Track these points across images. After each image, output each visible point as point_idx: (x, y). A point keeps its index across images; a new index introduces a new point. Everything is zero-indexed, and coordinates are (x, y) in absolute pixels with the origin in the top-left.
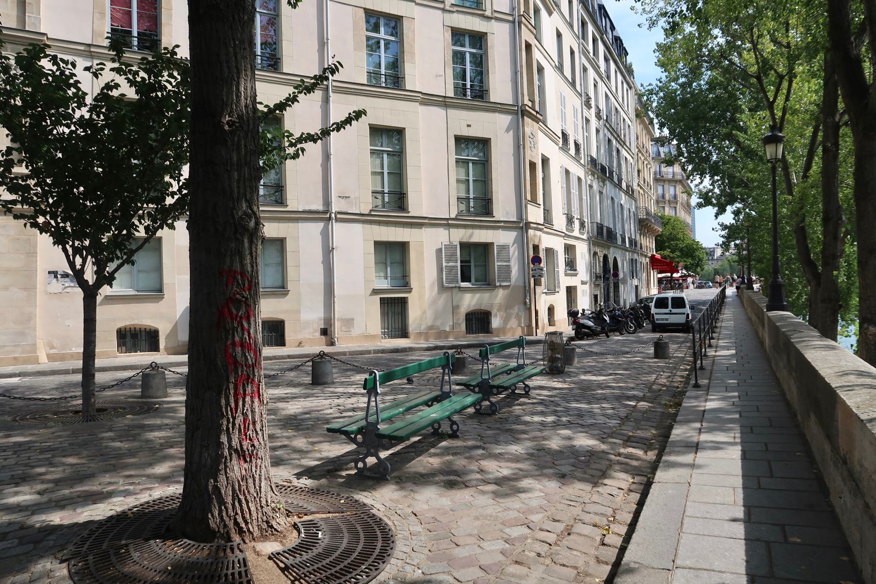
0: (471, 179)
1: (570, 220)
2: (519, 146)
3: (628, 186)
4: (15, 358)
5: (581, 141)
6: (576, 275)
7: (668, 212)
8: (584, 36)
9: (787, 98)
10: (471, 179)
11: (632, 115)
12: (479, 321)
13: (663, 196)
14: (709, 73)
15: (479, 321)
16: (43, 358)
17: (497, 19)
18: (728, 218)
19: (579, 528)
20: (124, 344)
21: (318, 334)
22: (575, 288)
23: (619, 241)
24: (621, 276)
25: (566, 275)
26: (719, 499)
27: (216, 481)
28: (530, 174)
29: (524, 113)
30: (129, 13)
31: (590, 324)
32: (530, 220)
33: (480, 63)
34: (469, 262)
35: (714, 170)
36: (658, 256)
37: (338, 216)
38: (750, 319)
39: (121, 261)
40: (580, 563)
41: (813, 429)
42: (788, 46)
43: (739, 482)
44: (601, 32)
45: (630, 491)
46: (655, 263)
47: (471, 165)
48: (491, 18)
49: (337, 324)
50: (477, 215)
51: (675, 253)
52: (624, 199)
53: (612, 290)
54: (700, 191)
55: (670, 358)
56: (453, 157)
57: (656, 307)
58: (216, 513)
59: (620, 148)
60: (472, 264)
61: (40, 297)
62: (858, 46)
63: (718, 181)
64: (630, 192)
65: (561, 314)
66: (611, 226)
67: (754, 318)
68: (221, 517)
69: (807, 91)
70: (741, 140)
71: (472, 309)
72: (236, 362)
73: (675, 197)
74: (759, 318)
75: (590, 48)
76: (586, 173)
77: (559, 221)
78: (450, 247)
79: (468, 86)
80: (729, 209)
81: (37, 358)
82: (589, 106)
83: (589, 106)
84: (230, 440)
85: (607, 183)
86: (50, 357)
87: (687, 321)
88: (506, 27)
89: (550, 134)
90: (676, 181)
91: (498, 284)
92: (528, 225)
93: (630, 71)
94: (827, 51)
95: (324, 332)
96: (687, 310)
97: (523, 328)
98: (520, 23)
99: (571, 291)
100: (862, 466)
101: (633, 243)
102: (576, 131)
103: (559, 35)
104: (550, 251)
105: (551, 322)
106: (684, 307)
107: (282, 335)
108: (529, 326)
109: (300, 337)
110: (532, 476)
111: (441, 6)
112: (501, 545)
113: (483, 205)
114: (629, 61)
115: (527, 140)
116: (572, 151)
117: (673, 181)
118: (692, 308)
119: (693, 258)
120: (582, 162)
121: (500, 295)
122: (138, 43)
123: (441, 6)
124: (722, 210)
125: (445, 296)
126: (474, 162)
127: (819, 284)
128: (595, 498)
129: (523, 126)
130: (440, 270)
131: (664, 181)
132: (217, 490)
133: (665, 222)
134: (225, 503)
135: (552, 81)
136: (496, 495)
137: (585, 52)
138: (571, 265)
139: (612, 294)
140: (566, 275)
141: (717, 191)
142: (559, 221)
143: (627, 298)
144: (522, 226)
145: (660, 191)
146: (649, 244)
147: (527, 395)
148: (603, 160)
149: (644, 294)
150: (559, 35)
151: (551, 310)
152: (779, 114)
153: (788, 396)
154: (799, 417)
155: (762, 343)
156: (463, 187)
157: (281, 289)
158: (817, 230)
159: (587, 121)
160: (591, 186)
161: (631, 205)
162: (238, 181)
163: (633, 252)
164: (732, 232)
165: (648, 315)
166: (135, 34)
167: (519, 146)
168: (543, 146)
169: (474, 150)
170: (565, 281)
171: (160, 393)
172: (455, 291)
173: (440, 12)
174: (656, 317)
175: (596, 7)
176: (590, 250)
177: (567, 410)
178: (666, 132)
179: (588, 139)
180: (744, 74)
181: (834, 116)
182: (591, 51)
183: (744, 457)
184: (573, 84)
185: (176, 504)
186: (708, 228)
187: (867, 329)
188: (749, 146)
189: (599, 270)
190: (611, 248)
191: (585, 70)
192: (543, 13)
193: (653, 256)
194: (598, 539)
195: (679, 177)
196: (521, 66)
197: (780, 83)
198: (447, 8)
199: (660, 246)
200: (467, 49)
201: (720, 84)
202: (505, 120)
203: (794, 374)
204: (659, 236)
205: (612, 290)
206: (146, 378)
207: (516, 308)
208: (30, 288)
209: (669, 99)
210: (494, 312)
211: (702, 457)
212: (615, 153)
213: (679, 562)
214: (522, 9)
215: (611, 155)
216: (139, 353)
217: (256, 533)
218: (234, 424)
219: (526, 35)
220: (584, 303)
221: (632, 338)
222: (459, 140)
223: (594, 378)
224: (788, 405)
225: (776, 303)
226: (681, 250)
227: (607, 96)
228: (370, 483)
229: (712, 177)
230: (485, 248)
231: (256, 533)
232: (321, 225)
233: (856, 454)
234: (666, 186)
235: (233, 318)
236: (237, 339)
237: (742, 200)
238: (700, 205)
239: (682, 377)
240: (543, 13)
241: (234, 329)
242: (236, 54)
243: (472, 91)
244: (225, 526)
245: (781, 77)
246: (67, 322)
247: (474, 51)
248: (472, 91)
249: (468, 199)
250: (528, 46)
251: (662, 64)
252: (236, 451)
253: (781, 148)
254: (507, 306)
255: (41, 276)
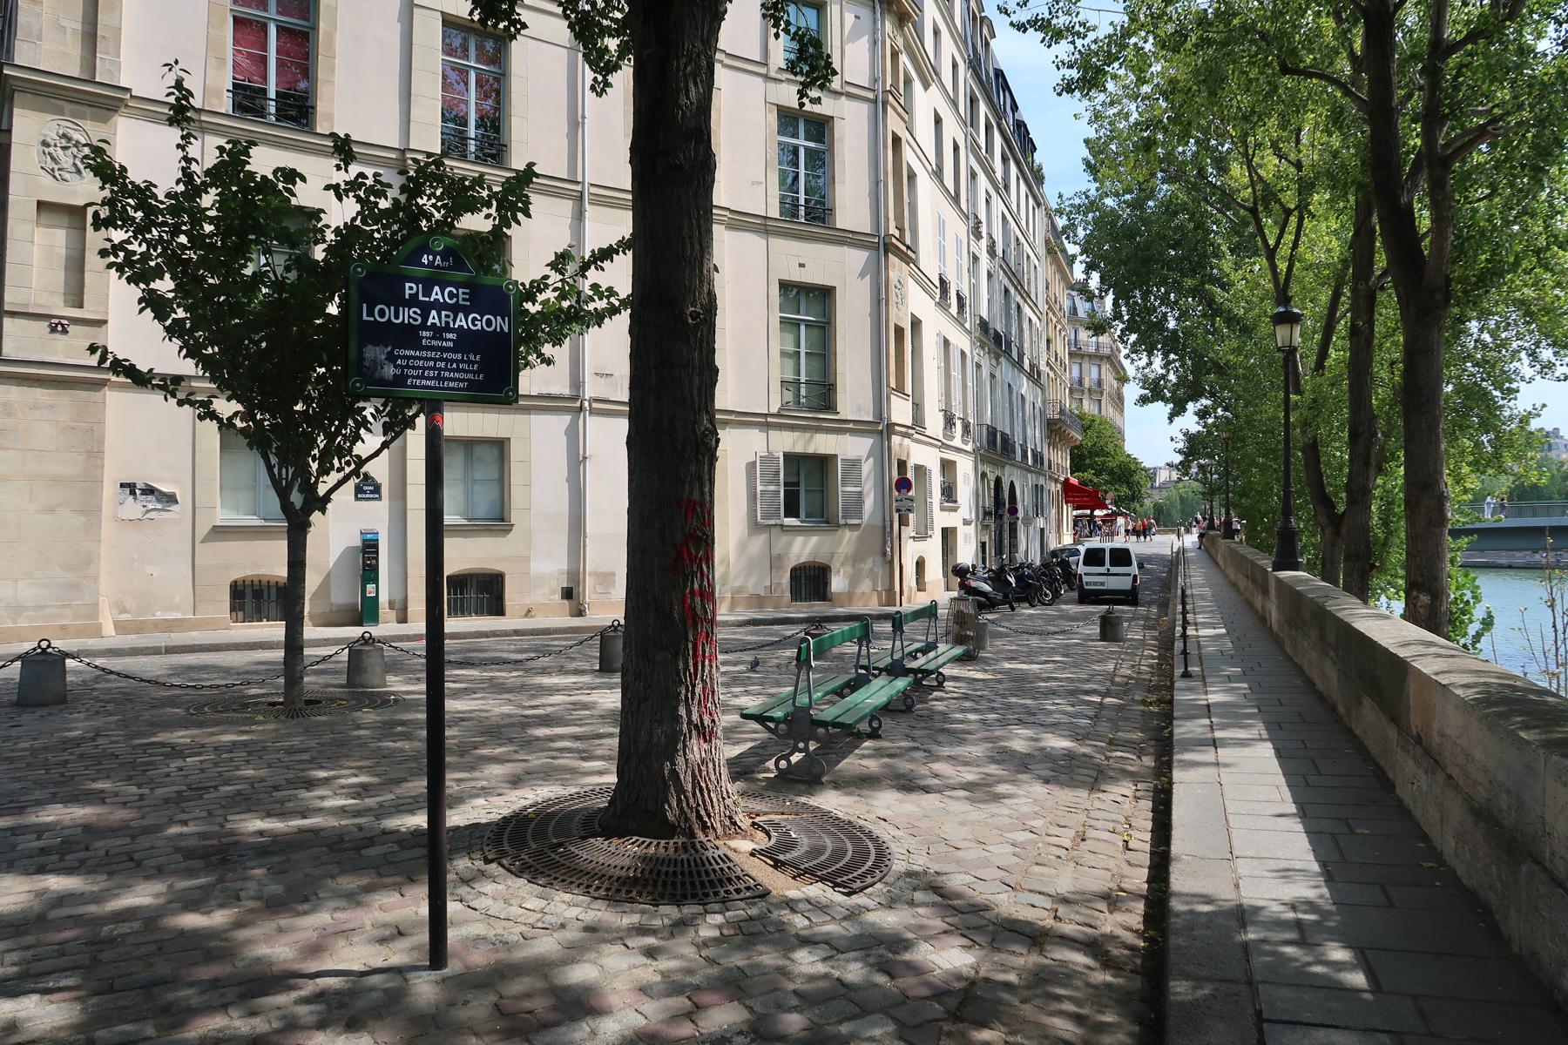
0: (803, 350)
1: (949, 422)
2: (880, 300)
3: (1032, 366)
4: (63, 627)
5: (966, 293)
6: (955, 510)
7: (1088, 407)
8: (974, 122)
9: (1295, 245)
10: (803, 350)
11: (1041, 250)
12: (811, 581)
13: (1080, 382)
14: (1165, 187)
15: (811, 581)
16: (108, 628)
17: (850, 96)
18: (1189, 421)
19: (1091, 833)
20: (242, 608)
21: (557, 597)
22: (954, 530)
23: (1019, 458)
24: (1020, 514)
25: (942, 509)
26: (1262, 797)
27: (673, 764)
28: (895, 343)
29: (888, 248)
30: (264, 60)
31: (987, 588)
32: (895, 419)
33: (821, 161)
34: (797, 484)
35: (1172, 344)
36: (1074, 481)
37: (595, 405)
38: (1234, 585)
39: (342, 474)
40: (1111, 864)
41: (1368, 719)
42: (1298, 165)
43: (1282, 780)
44: (998, 113)
45: (1137, 798)
46: (1071, 493)
47: (803, 328)
48: (841, 94)
49: (589, 582)
50: (811, 409)
51: (1101, 478)
52: (1025, 386)
53: (1006, 535)
54: (1145, 376)
55: (1124, 641)
56: (776, 315)
57: (1085, 564)
58: (675, 804)
59: (1021, 302)
60: (802, 489)
61: (107, 527)
62: (1411, 192)
63: (1174, 361)
64: (1034, 376)
65: (934, 571)
66: (1008, 431)
67: (1243, 582)
68: (681, 809)
69: (1325, 237)
70: (1219, 300)
71: (802, 560)
72: (695, 615)
73: (1100, 383)
74: (1254, 581)
75: (982, 141)
76: (973, 344)
77: (934, 423)
78: (768, 459)
79: (802, 202)
80: (1190, 406)
81: (99, 628)
82: (978, 236)
83: (978, 236)
84: (689, 713)
85: (1002, 359)
86: (121, 627)
87: (1134, 587)
88: (863, 109)
89: (922, 281)
90: (1101, 358)
91: (842, 522)
92: (891, 428)
93: (1038, 177)
94: (1360, 187)
95: (568, 594)
96: (1134, 569)
97: (879, 594)
98: (885, 103)
99: (948, 535)
100: (1442, 735)
101: (1038, 458)
102: (959, 277)
103: (938, 121)
104: (920, 469)
105: (921, 586)
106: (1129, 564)
107: (500, 598)
108: (890, 590)
109: (529, 601)
110: (1006, 781)
111: (763, 70)
112: (1009, 849)
113: (823, 394)
114: (1037, 161)
115: (892, 291)
116: (954, 310)
117: (1097, 358)
118: (1141, 566)
119: (1130, 485)
120: (967, 325)
121: (846, 541)
122: (277, 109)
123: (763, 70)
124: (1179, 410)
125: (759, 541)
126: (809, 325)
127: (1337, 533)
128: (1097, 804)
129: (887, 268)
130: (752, 497)
131: (1082, 356)
132: (674, 773)
133: (1087, 425)
134: (684, 792)
135: (928, 194)
136: (971, 800)
137: (974, 148)
138: (949, 492)
139: (1006, 542)
140: (942, 509)
141: (1172, 377)
142: (934, 423)
143: (1029, 551)
144: (881, 429)
145: (1076, 373)
146: (1060, 460)
147: (940, 686)
148: (999, 327)
149: (1053, 545)
150: (938, 121)
151: (920, 565)
152: (1282, 266)
153: (1320, 686)
154: (1341, 710)
155: (1263, 619)
156: (790, 363)
157: (498, 521)
158: (1338, 452)
159: (976, 259)
160: (978, 366)
161: (1036, 397)
162: (700, 388)
163: (1040, 473)
164: (1193, 446)
165: (1070, 577)
166: (272, 94)
167: (880, 300)
168: (917, 302)
169: (809, 303)
170: (941, 519)
171: (376, 681)
172: (774, 531)
173: (760, 80)
174: (1085, 579)
175: (992, 74)
176: (976, 469)
177: (1009, 707)
178: (1095, 280)
179: (974, 288)
180: (1227, 198)
181: (1367, 280)
182: (983, 146)
183: (1279, 754)
184: (956, 199)
185: (602, 803)
186: (1153, 437)
187: (1417, 598)
188: (1230, 311)
189: (989, 503)
190: (1007, 468)
191: (973, 175)
192: (917, 85)
193: (1066, 483)
194: (1121, 844)
195: (1107, 351)
196: (886, 173)
197: (1286, 221)
198: (773, 74)
199: (1077, 465)
200: (801, 142)
201: (1184, 208)
202: (857, 258)
203: (1332, 653)
204: (1077, 447)
205: (1006, 535)
206: (355, 656)
207: (870, 561)
208: (90, 510)
209: (1106, 225)
210: (835, 566)
211: (1224, 754)
212: (1014, 312)
213: (1236, 853)
214: (889, 82)
215: (1008, 316)
216: (265, 622)
217: (720, 830)
218: (693, 693)
219: (894, 124)
220: (966, 554)
221: (1050, 611)
222: (785, 286)
223: (1025, 666)
224: (1321, 697)
225: (1287, 560)
226: (1111, 472)
227: (1004, 218)
228: (802, 787)
229: (1165, 355)
230: (822, 464)
231: (720, 830)
232: (567, 418)
233: (1436, 726)
234: (1086, 365)
235: (693, 559)
236: (696, 586)
237: (1212, 395)
238: (1144, 400)
239: (1151, 666)
240: (917, 85)
241: (693, 574)
242: (699, 227)
243: (809, 211)
244: (687, 819)
245: (1288, 212)
246: (149, 569)
247: (812, 145)
248: (809, 211)
249: (798, 382)
250: (897, 140)
251: (1091, 168)
252: (696, 726)
253: (1297, 329)
254: (856, 558)
255: (110, 491)
